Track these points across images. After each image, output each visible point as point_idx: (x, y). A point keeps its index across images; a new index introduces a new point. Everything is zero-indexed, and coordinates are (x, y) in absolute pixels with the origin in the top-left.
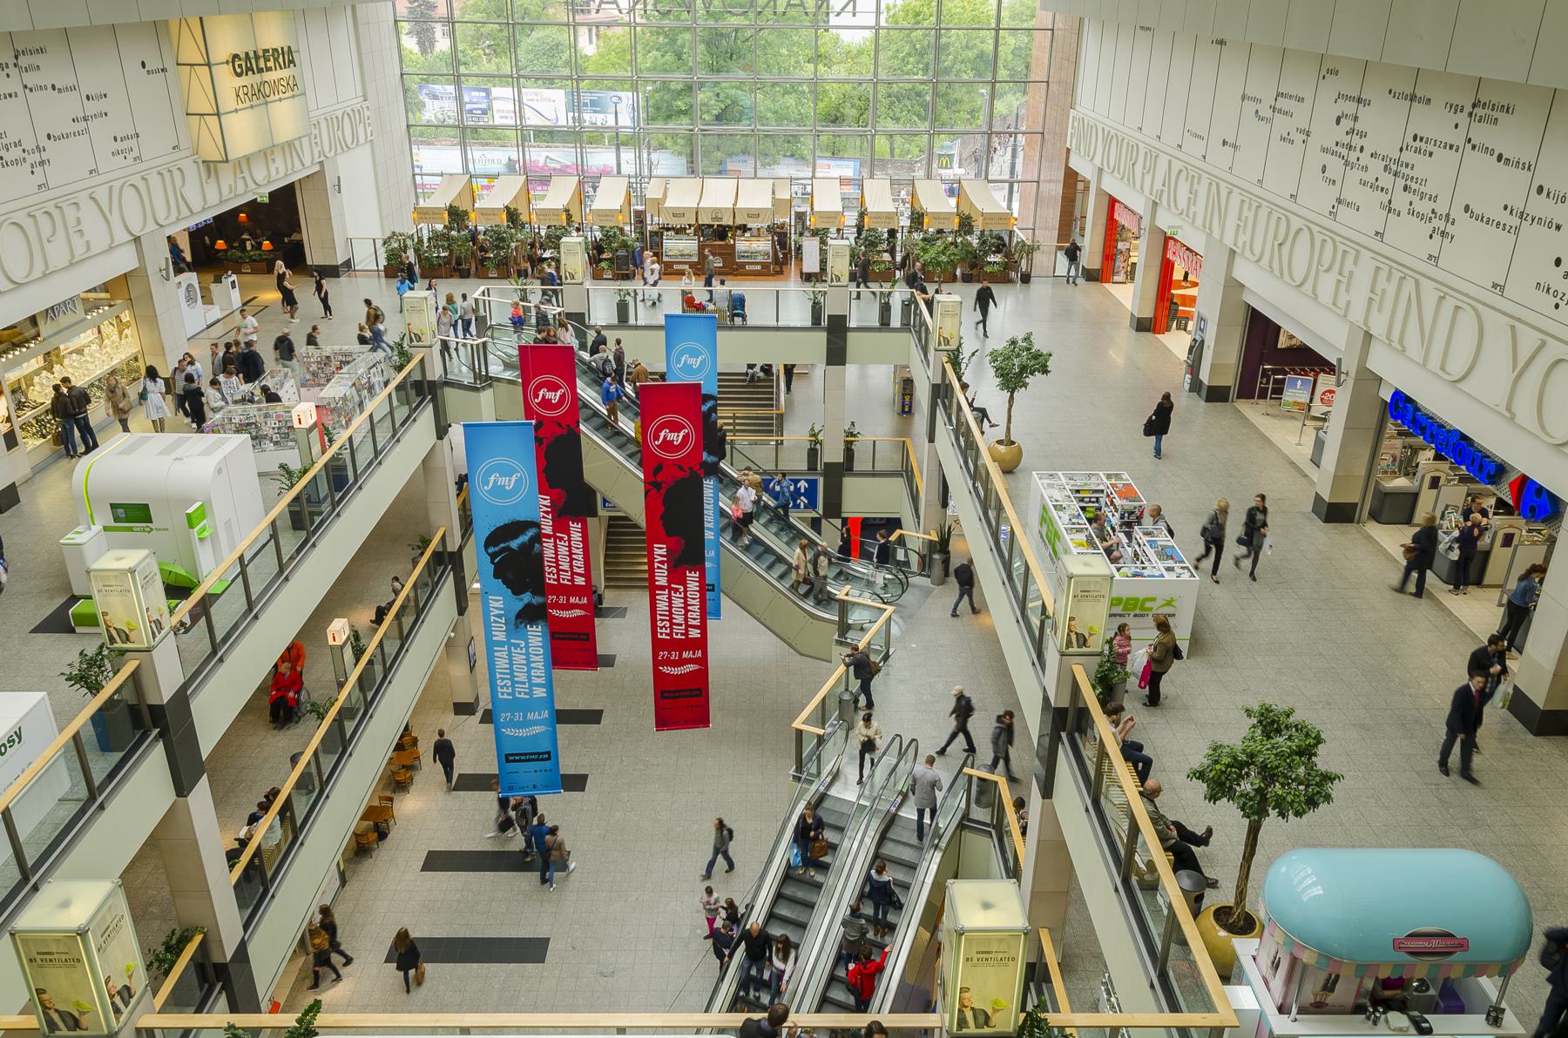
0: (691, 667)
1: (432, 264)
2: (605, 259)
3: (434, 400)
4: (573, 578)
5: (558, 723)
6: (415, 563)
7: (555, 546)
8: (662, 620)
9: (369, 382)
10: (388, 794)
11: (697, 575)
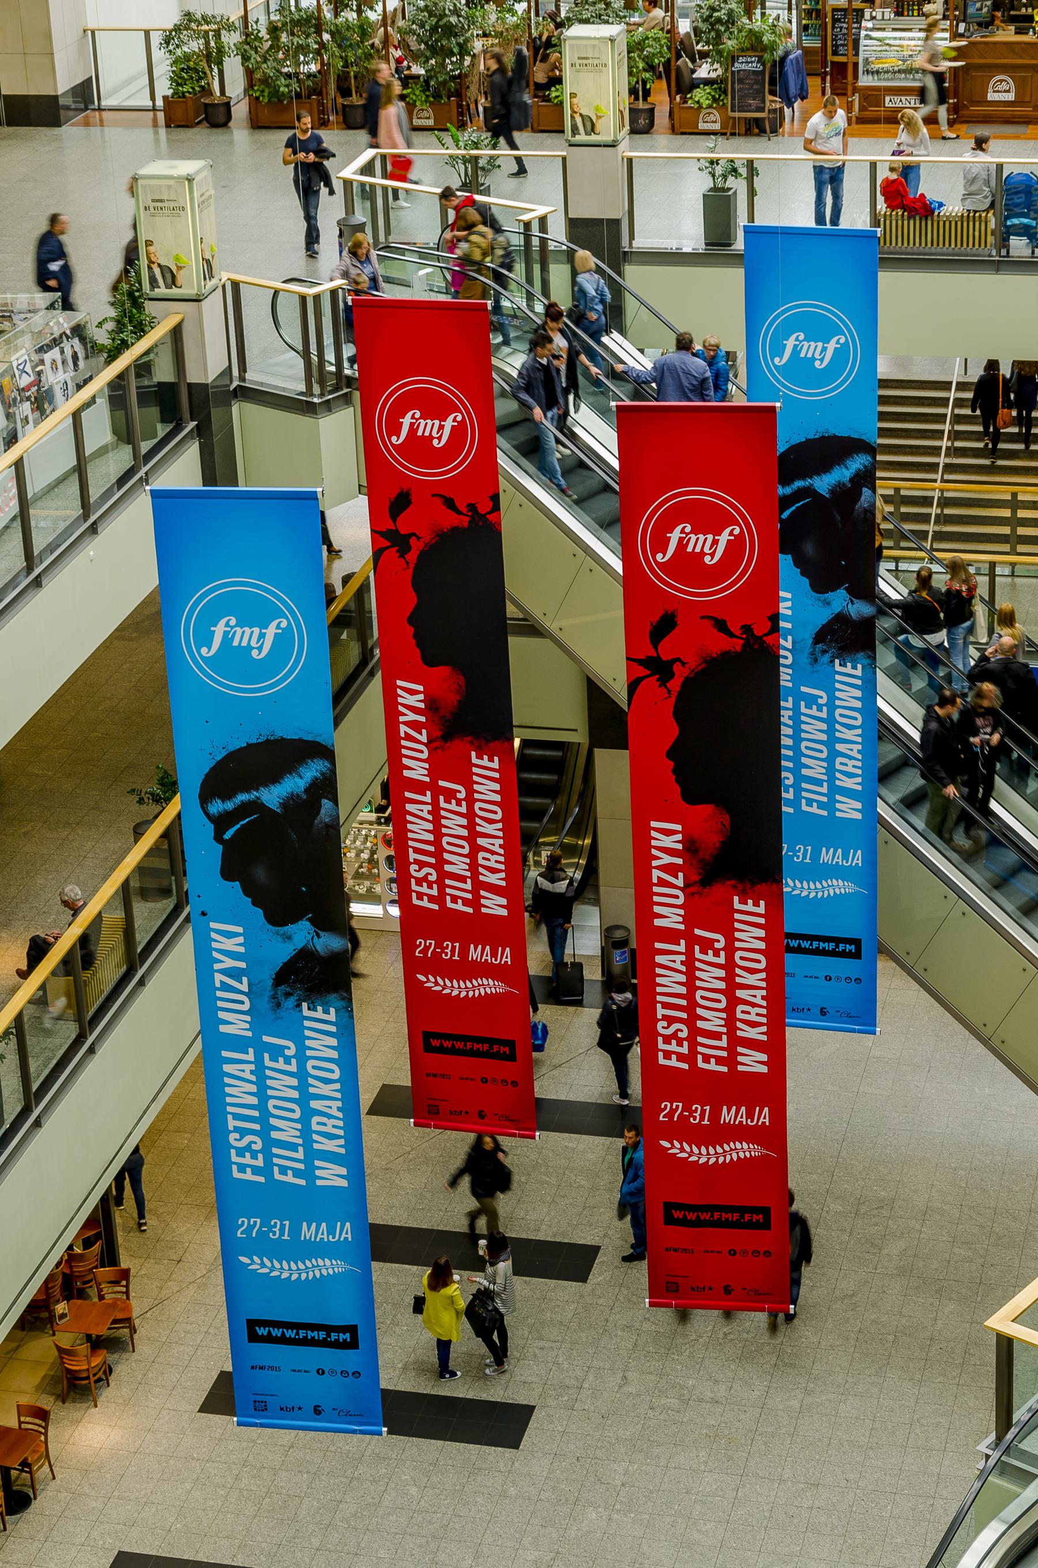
0: (743, 1150)
1: (275, 93)
2: (707, 82)
3: (203, 432)
4: (477, 897)
5: (373, 1260)
6: (138, 832)
7: (436, 811)
8: (670, 1020)
9: (38, 382)
10: (46, 1402)
11: (761, 909)
